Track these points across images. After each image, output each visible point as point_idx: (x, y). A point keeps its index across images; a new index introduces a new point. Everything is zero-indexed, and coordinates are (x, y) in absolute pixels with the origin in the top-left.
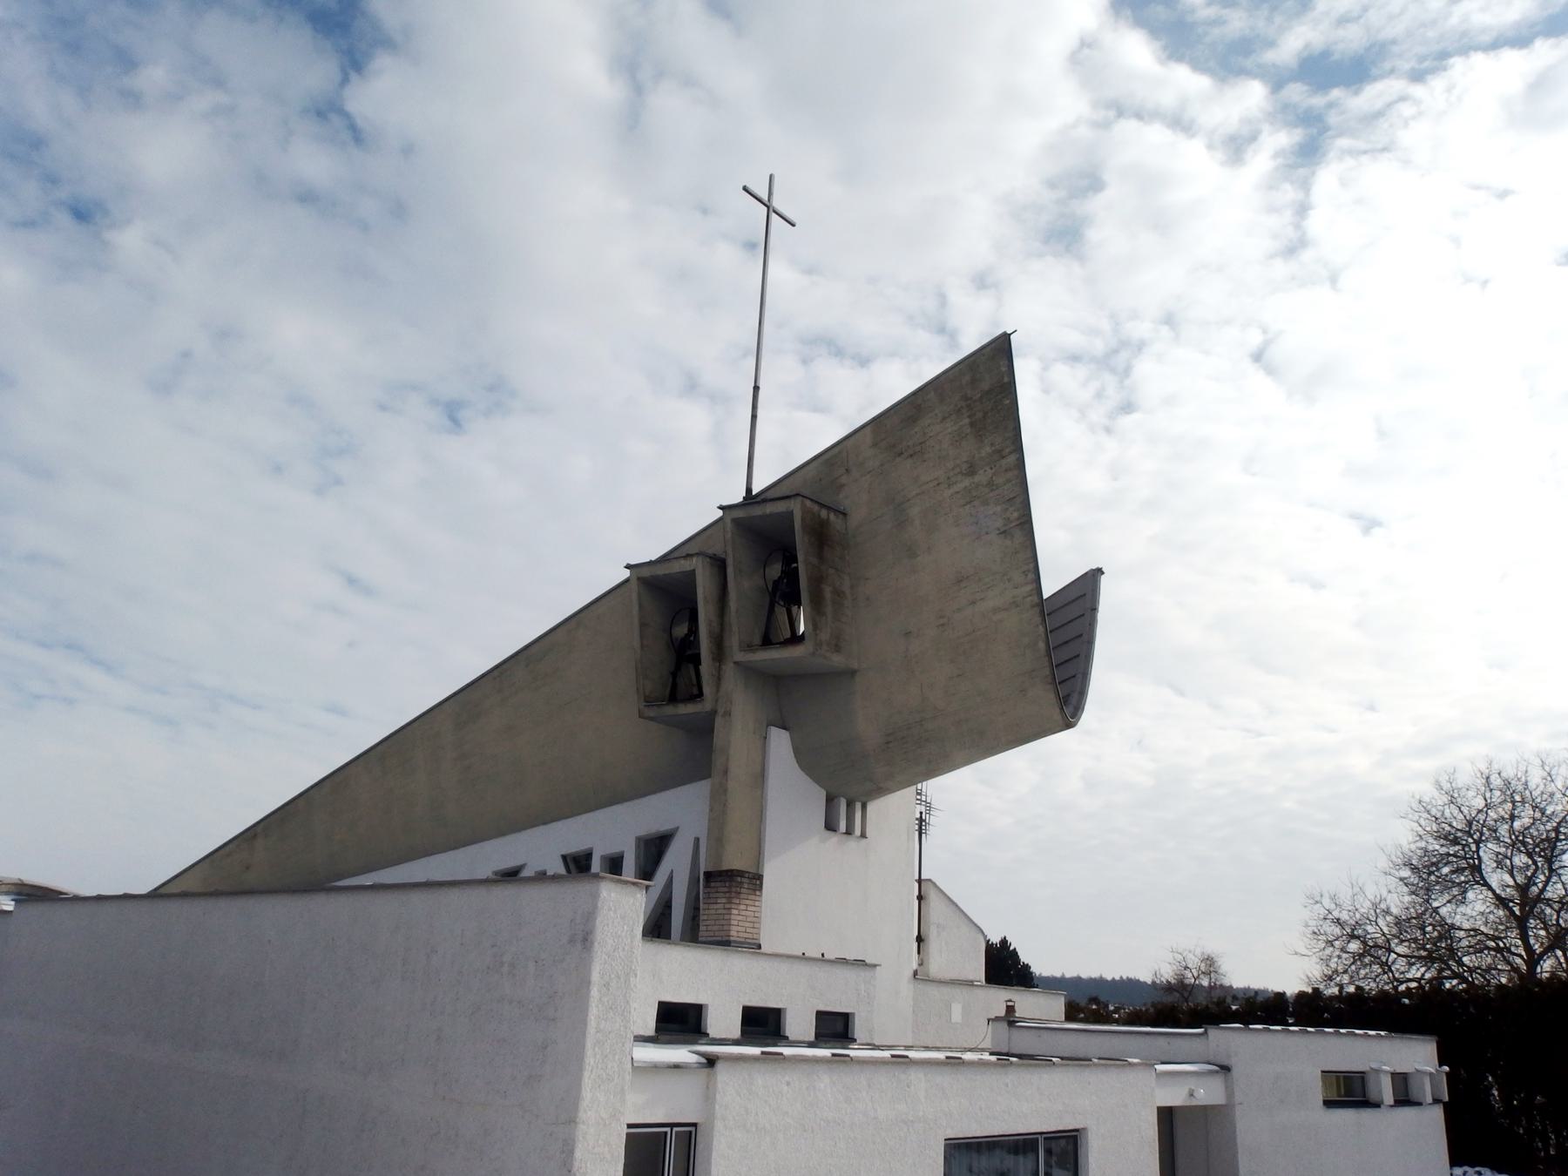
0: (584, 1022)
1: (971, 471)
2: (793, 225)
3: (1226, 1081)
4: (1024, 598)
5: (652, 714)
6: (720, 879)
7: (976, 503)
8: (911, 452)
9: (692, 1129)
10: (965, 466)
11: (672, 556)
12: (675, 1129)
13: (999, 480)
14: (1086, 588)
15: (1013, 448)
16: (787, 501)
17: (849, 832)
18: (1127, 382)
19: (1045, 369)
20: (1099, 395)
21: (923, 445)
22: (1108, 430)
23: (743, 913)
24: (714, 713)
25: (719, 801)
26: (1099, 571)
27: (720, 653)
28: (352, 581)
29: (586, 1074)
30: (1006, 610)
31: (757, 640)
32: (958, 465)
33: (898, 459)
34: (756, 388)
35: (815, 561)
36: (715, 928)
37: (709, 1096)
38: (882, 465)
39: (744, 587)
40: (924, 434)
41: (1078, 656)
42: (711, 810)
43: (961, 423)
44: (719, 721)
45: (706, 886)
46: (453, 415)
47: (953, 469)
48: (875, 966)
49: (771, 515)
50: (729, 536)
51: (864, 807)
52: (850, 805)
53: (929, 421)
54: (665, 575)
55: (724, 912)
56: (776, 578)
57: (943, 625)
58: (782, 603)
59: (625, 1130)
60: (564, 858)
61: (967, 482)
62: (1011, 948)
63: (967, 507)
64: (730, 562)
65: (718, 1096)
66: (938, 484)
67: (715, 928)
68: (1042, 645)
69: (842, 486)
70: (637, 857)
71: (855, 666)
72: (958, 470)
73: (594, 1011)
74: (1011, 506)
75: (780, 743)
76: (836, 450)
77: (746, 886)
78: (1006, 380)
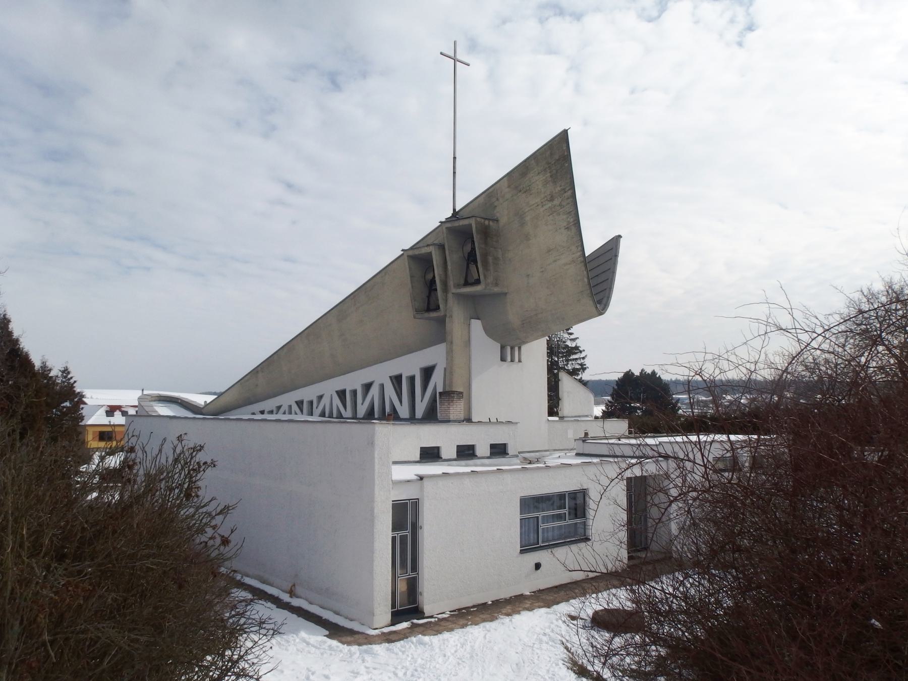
0: (374, 470)
1: (552, 199)
2: (468, 65)
3: (667, 462)
4: (577, 258)
5: (419, 317)
6: (444, 395)
8: (525, 190)
9: (417, 500)
10: (549, 197)
11: (418, 246)
12: (410, 501)
13: (564, 203)
14: (611, 250)
15: (569, 187)
16: (469, 219)
17: (512, 361)
18: (751, 9)
19: (695, 7)
20: (732, 21)
22: (740, 44)
23: (455, 408)
24: (445, 316)
25: (450, 353)
26: (620, 236)
27: (446, 289)
28: (290, 186)
29: (376, 487)
30: (569, 264)
31: (462, 282)
32: (546, 196)
34: (455, 158)
35: (483, 246)
36: (445, 415)
37: (422, 489)
38: (512, 197)
39: (454, 258)
40: (530, 181)
41: (608, 279)
42: (447, 360)
44: (447, 320)
45: (440, 398)
46: (334, 82)
48: (517, 423)
50: (445, 235)
51: (520, 348)
52: (512, 349)
55: (447, 408)
56: (469, 251)
57: (542, 272)
58: (473, 263)
59: (391, 502)
60: (390, 377)
61: (550, 204)
62: (657, 376)
63: (551, 216)
64: (446, 247)
65: (425, 490)
66: (538, 205)
67: (445, 415)
68: (586, 280)
69: (496, 206)
70: (421, 377)
71: (505, 290)
72: (546, 199)
73: (377, 467)
74: (570, 216)
75: (477, 326)
76: (491, 190)
77: (456, 397)
78: (566, 154)
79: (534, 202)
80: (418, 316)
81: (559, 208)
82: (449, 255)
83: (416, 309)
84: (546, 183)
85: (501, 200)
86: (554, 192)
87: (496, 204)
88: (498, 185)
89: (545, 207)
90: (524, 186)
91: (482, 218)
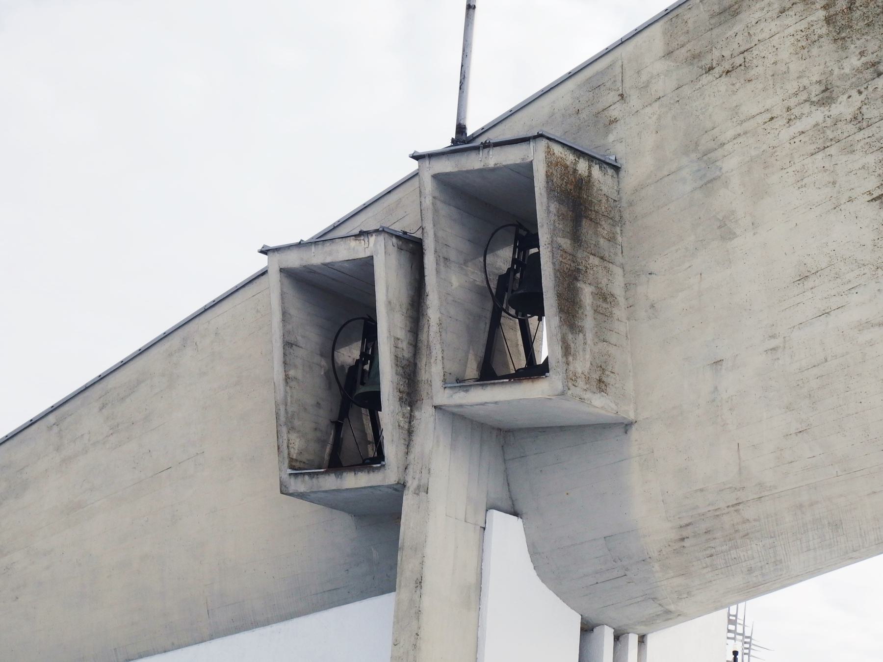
1: (827, 96)
7: (833, 150)
8: (727, 66)
16: (523, 147)
21: (596, 91)
24: (400, 487)
31: (472, 371)
33: (706, 79)
35: (566, 243)
44: (409, 501)
50: (428, 201)
51: (642, 640)
53: (758, 15)
58: (512, 311)
61: (818, 115)
63: (820, 156)
64: (429, 246)
66: (772, 119)
69: (614, 121)
72: (803, 96)
79: (754, 110)
80: (300, 485)
81: (851, 128)
82: (438, 272)
83: (291, 460)
84: (810, 40)
85: (635, 101)
86: (836, 71)
87: (614, 112)
88: (630, 46)
89: (799, 126)
90: (727, 53)
91: (571, 148)
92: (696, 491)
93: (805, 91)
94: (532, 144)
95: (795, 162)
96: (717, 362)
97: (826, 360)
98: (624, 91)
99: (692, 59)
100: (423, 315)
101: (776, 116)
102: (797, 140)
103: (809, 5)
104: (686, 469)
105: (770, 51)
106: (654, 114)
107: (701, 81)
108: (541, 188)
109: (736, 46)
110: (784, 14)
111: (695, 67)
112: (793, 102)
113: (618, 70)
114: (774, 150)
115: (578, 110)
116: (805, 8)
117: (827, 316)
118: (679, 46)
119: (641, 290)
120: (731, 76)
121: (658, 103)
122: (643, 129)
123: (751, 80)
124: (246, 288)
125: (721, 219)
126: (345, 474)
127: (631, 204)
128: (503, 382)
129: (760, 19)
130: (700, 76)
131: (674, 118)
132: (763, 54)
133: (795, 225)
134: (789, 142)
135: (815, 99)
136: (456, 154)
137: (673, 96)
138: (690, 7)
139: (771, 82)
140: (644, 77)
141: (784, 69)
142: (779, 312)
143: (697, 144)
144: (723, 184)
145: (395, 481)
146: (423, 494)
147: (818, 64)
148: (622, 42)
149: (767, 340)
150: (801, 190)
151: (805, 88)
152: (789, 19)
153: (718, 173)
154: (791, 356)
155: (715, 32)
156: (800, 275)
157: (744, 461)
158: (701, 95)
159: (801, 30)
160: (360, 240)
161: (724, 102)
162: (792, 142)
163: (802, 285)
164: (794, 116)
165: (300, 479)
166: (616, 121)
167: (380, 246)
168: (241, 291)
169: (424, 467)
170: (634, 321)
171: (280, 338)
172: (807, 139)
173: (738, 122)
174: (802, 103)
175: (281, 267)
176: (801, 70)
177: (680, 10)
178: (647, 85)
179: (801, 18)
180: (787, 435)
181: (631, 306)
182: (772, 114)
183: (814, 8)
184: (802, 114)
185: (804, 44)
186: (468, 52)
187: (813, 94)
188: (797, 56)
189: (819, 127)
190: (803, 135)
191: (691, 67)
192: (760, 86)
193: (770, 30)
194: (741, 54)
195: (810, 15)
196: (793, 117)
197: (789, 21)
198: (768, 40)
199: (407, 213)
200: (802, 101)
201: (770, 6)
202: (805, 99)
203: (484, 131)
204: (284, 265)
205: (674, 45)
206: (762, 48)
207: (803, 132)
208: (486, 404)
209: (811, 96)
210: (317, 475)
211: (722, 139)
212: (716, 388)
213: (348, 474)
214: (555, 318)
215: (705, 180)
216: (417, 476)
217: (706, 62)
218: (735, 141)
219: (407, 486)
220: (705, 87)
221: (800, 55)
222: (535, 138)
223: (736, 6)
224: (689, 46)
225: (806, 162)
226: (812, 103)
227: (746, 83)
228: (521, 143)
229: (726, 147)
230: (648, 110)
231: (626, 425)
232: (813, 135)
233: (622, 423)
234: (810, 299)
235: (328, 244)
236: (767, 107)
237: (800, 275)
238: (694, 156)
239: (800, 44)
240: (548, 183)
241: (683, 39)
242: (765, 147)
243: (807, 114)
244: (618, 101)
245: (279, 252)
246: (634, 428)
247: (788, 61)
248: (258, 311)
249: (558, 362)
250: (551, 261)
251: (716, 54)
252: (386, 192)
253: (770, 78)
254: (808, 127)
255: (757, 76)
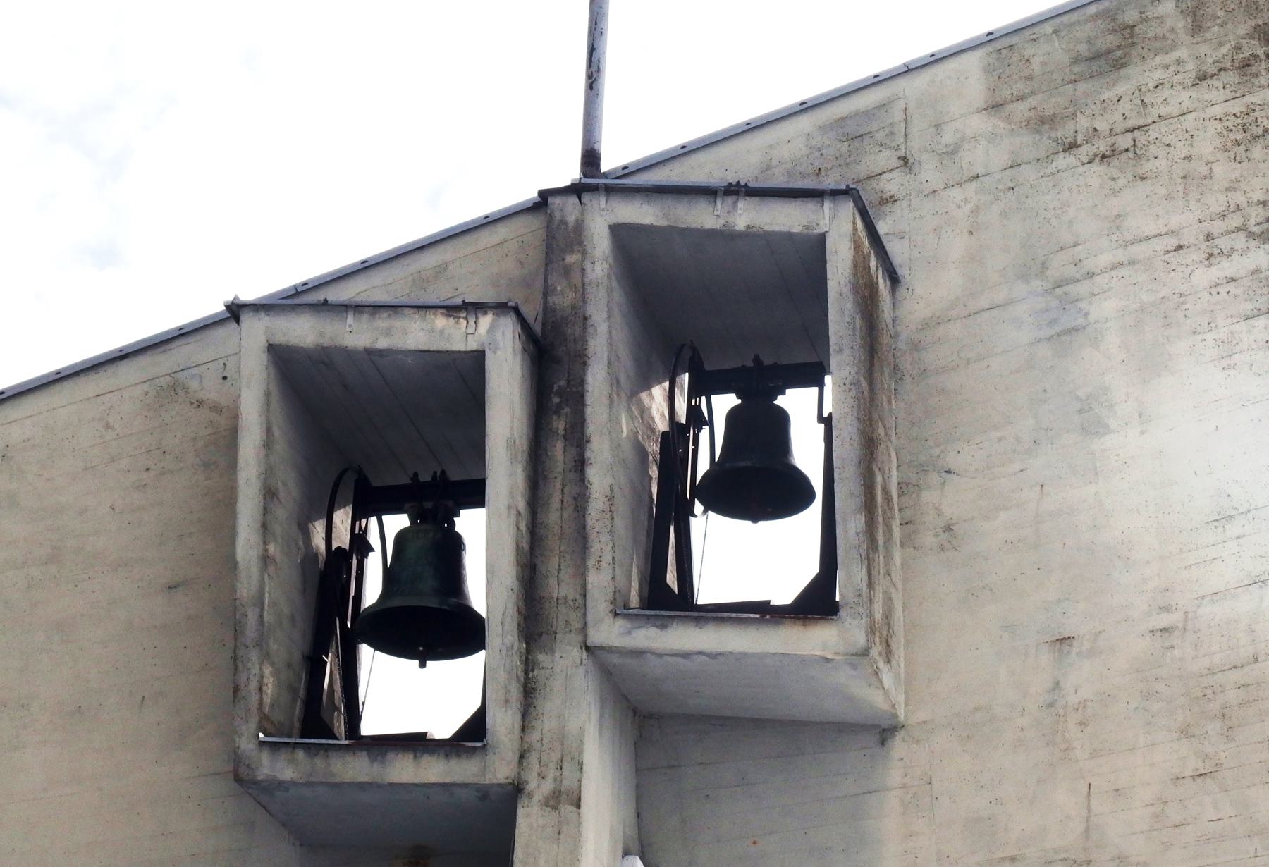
8: (1103, 146)
21: (857, 143)
24: (515, 791)
33: (1063, 161)
43: (1250, 99)
47: (1223, 216)
49: (750, 235)
53: (1158, 75)
54: (370, 352)
66: (1180, 247)
72: (1235, 221)
79: (1150, 228)
85: (929, 174)
90: (1102, 126)
92: (1003, 859)
93: (1238, 213)
94: (828, 205)
95: (1219, 326)
96: (1063, 639)
97: (1256, 660)
98: (908, 152)
99: (1039, 123)
100: (546, 478)
101: (1186, 244)
102: (1223, 290)
103: (1248, 78)
104: (989, 819)
105: (1180, 138)
106: (966, 201)
107: (1054, 163)
108: (842, 282)
109: (1118, 117)
110: (1204, 83)
111: (1045, 138)
112: (1217, 227)
113: (898, 116)
114: (1182, 299)
115: (820, 169)
116: (1240, 81)
117: (1261, 587)
118: (1014, 99)
119: (928, 497)
120: (1109, 165)
121: (974, 183)
122: (946, 223)
123: (1146, 178)
124: (82, 380)
125: (1084, 398)
126: (390, 755)
127: (916, 347)
128: (338, 651)
129: (1161, 81)
130: (1053, 154)
131: (1004, 215)
132: (1167, 140)
133: (1215, 427)
134: (1209, 290)
135: (1256, 229)
136: (665, 196)
137: (1002, 179)
138: (1035, 36)
139: (1180, 188)
140: (948, 137)
141: (1205, 170)
142: (1179, 568)
143: (1044, 266)
144: (1090, 340)
145: (507, 778)
146: (568, 809)
147: (1262, 174)
148: (908, 70)
149: (1154, 613)
150: (1227, 372)
151: (1238, 208)
152: (1215, 92)
153: (1081, 321)
154: (1196, 645)
155: (1082, 87)
156: (1219, 513)
157: (1096, 815)
158: (1054, 186)
159: (1234, 115)
160: (460, 318)
161: (1096, 205)
162: (1214, 291)
163: (1220, 529)
164: (1219, 251)
165: (283, 755)
166: (892, 200)
167: (503, 333)
168: (68, 384)
169: (567, 759)
170: (912, 549)
171: (258, 478)
172: (1239, 291)
173: (1120, 242)
174: (1233, 232)
175: (271, 342)
176: (1233, 178)
177: (1015, 40)
178: (952, 152)
179: (1234, 95)
180: (1178, 778)
181: (907, 524)
182: (1179, 240)
183: (1257, 83)
184: (1233, 250)
185: (1239, 137)
186: (602, 27)
187: (1252, 221)
188: (1226, 154)
189: (1262, 276)
190: (1233, 283)
191: (1037, 137)
192: (1163, 191)
193: (1180, 104)
194: (1127, 131)
195: (1250, 93)
196: (1216, 251)
197: (1213, 95)
198: (1176, 119)
199: (459, 292)
200: (1233, 229)
201: (1179, 64)
202: (1238, 226)
203: (627, 172)
204: (280, 339)
205: (1006, 93)
206: (1166, 129)
207: (1233, 280)
208: (718, 656)
209: (1248, 223)
210: (326, 750)
211: (1089, 265)
212: (1057, 685)
213: (400, 756)
214: (858, 516)
215: (1057, 329)
216: (552, 773)
217: (1065, 132)
218: (1114, 273)
219: (526, 792)
220: (1061, 173)
221: (1232, 154)
222: (835, 194)
223: (1119, 53)
224: (1033, 101)
225: (1237, 327)
226: (1251, 235)
227: (1136, 181)
228: (805, 199)
229: (1098, 280)
230: (956, 193)
231: (884, 730)
232: (1249, 287)
233: (878, 726)
234: (1234, 554)
235: (385, 315)
236: (1172, 226)
237: (1219, 513)
238: (1037, 284)
239: (1232, 136)
240: (612, 291)
241: (1020, 87)
242: (1165, 292)
243: (1240, 250)
244: (897, 168)
245: (272, 313)
246: (900, 736)
247: (1211, 159)
248: (108, 426)
249: (860, 595)
250: (856, 414)
251: (1083, 123)
252: (415, 247)
253: (1180, 181)
254: (1243, 273)
255: (1155, 172)
